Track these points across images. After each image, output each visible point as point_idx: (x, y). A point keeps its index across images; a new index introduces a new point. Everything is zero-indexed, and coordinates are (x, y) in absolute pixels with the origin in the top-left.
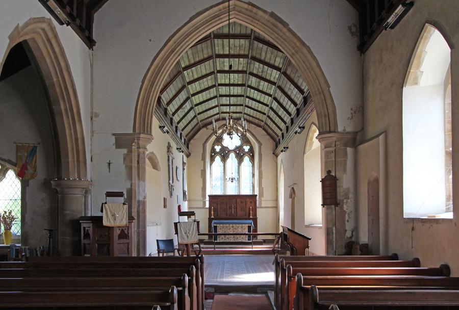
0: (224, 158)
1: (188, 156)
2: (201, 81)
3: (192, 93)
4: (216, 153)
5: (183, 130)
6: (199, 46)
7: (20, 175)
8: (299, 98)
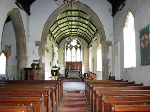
0: (71, 49)
1: (59, 48)
2: (63, 24)
3: (60, 27)
4: (68, 47)
5: (57, 40)
6: (63, 14)
7: (6, 55)
8: (95, 30)
